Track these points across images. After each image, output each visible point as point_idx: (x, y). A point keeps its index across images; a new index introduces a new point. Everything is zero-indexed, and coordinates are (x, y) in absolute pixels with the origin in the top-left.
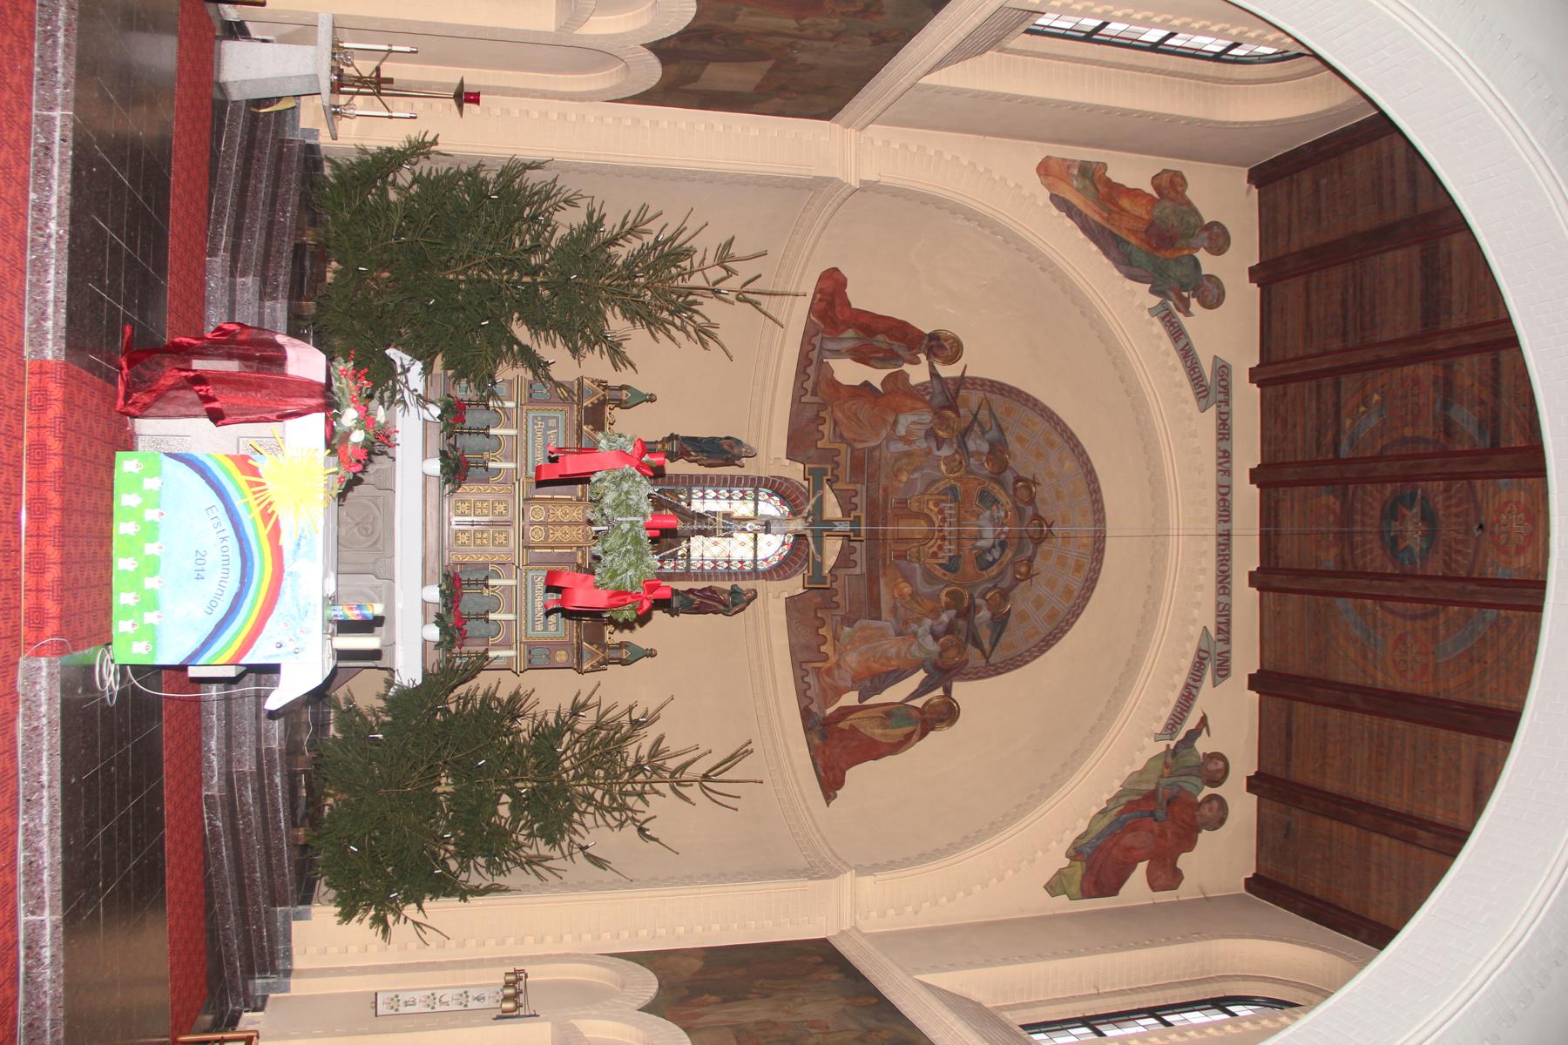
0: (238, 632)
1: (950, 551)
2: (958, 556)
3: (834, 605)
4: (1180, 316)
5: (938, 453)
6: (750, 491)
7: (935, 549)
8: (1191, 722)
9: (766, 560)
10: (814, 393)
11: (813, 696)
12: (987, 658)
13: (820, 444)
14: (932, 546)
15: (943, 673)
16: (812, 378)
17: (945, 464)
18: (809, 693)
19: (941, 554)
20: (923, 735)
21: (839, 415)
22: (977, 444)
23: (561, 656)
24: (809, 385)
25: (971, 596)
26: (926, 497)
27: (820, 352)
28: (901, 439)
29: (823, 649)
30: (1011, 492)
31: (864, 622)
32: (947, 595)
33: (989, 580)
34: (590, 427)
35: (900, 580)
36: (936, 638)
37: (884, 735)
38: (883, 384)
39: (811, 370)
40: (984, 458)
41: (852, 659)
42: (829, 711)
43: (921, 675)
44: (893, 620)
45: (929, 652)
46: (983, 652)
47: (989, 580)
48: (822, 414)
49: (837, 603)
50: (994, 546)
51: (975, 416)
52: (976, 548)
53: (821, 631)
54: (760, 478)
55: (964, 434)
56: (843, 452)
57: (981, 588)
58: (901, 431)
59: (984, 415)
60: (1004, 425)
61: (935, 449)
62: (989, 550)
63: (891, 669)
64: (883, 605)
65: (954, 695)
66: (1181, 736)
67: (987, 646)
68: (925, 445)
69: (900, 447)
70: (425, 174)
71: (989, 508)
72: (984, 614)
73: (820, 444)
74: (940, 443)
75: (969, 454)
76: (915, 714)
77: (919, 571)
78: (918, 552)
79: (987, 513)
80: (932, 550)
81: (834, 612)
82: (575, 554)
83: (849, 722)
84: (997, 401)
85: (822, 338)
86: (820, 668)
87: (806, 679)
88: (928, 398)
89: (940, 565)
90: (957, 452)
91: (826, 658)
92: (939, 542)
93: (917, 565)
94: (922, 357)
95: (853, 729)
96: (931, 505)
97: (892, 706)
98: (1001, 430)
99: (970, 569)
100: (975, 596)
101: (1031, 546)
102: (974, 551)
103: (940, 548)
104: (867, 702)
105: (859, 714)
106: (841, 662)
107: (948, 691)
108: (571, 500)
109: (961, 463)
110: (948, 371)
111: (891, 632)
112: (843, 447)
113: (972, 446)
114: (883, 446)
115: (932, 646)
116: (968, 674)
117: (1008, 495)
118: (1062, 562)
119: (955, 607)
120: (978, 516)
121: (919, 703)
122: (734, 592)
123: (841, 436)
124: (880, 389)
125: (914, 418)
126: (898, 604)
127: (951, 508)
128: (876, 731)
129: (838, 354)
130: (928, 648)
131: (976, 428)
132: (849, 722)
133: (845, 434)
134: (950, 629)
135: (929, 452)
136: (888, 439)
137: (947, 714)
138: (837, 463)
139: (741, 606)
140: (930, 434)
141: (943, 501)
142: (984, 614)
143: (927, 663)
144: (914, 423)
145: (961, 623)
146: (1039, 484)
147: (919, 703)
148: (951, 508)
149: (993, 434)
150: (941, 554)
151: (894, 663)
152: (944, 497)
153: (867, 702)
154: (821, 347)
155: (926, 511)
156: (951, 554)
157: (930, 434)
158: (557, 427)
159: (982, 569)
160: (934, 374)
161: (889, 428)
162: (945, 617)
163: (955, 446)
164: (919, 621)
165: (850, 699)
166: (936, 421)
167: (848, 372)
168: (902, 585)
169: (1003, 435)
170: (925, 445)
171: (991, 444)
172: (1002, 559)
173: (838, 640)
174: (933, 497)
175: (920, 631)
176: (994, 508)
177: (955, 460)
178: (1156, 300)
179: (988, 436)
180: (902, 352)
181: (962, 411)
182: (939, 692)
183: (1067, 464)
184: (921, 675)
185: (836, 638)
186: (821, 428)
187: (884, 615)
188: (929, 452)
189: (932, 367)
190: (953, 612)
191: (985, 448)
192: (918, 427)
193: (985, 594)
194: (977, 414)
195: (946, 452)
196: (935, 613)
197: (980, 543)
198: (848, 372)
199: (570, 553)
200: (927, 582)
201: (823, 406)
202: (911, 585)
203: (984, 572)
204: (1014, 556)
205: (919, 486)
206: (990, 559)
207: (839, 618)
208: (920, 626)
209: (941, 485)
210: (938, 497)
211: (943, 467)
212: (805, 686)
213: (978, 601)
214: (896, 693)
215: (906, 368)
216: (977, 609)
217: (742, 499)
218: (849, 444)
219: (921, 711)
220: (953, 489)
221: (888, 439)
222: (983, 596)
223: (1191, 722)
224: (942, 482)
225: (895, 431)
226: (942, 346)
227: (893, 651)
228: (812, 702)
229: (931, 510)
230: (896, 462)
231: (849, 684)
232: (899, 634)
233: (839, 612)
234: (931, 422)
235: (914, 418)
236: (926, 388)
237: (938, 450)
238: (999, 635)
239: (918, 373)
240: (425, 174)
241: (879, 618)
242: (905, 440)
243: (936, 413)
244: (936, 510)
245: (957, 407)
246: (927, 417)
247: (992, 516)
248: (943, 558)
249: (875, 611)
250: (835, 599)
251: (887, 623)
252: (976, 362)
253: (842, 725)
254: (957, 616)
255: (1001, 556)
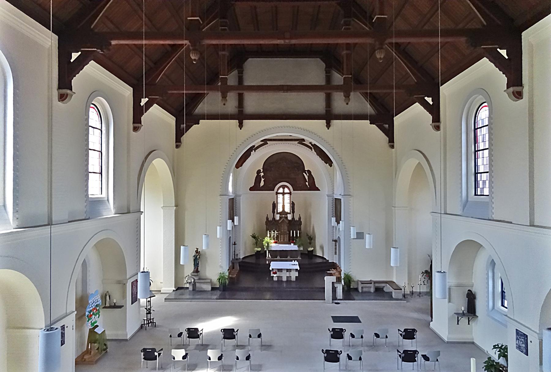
4: (255, 147)
8: (310, 145)
15: (305, 171)
22: (272, 165)
38: (263, 178)
65: (307, 170)
66: (312, 147)
70: (197, 55)
104: (308, 181)
107: (306, 171)
110: (262, 171)
115: (300, 172)
121: (308, 175)
122: (292, 204)
134: (298, 169)
137: (309, 172)
142: (296, 165)
147: (308, 175)
165: (307, 183)
167: (262, 184)
178: (253, 151)
182: (306, 172)
198: (262, 184)
214: (307, 178)
215: (261, 176)
223: (310, 145)
226: (259, 172)
239: (262, 174)
240: (197, 55)
252: (261, 168)
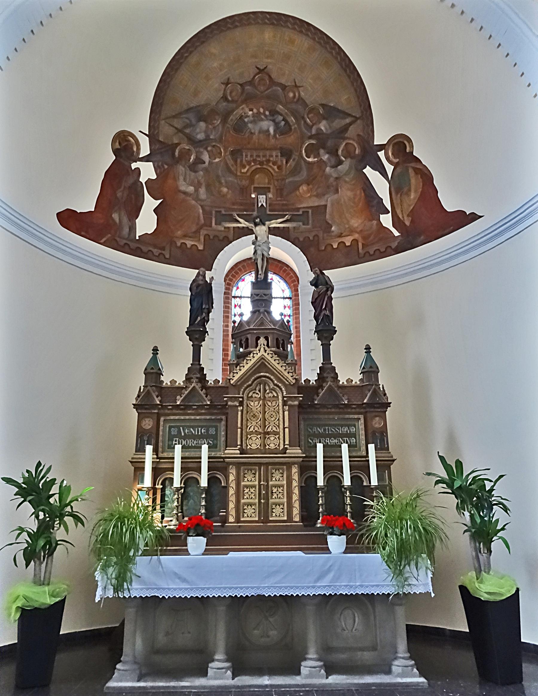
0: (281, 554)
1: (277, 156)
2: (281, 149)
3: (316, 238)
5: (207, 163)
6: (234, 301)
7: (275, 167)
9: (283, 291)
10: (163, 249)
11: (385, 246)
12: (357, 119)
13: (201, 247)
14: (274, 169)
16: (151, 249)
17: (215, 159)
18: (383, 250)
19: (279, 163)
20: (418, 160)
21: (179, 233)
23: (377, 423)
24: (156, 252)
25: (310, 137)
26: (239, 174)
27: (131, 241)
28: (196, 190)
29: (348, 244)
30: (234, 105)
31: (328, 216)
32: (309, 158)
33: (299, 125)
34: (178, 397)
35: (298, 193)
36: (340, 163)
37: (416, 191)
39: (145, 249)
40: (210, 126)
41: (356, 223)
42: (396, 233)
43: (368, 171)
44: (326, 197)
45: (350, 167)
46: (350, 124)
47: (299, 125)
48: (179, 244)
49: (314, 237)
50: (274, 121)
51: (179, 131)
52: (275, 135)
53: (335, 246)
54: (225, 293)
55: (191, 140)
56: (205, 232)
57: (304, 129)
58: (191, 189)
59: (178, 123)
60: (185, 107)
61: (204, 165)
62: (276, 124)
63: (363, 194)
64: (316, 204)
67: (348, 120)
68: (201, 173)
69: (202, 191)
71: (246, 124)
72: (323, 126)
73: (201, 247)
74: (199, 161)
75: (207, 138)
76: (399, 170)
77: (291, 179)
78: (277, 180)
79: (250, 125)
80: (277, 170)
81: (321, 238)
82: (290, 406)
83: (406, 218)
84: (167, 110)
85: (119, 237)
86: (363, 244)
87: (372, 253)
88: (166, 167)
89: (287, 163)
90: (206, 149)
91: (355, 241)
92: (271, 164)
93: (287, 181)
94: (134, 166)
95: (411, 214)
96: (246, 170)
97: (392, 189)
98: (189, 110)
99: (291, 139)
100: (309, 134)
101: (274, 88)
102: (277, 136)
103: (274, 163)
104: (390, 209)
105: (398, 211)
106: (359, 230)
107: (381, 147)
108: (242, 411)
109: (214, 146)
111: (336, 196)
112: (203, 232)
113: (201, 136)
114: (202, 204)
116: (369, 134)
117: (237, 108)
118: (287, 57)
119: (318, 150)
120: (252, 133)
121: (389, 169)
123: (195, 232)
124: (160, 201)
125: (181, 178)
126: (315, 193)
127: (246, 156)
128: (412, 197)
129: (133, 228)
130: (347, 168)
131: (187, 131)
132: (406, 218)
133: (194, 230)
135: (206, 170)
136: (197, 199)
138: (215, 236)
139: (327, 279)
140: (193, 168)
141: (241, 161)
142: (323, 126)
143: (359, 167)
144: (185, 180)
145: (330, 143)
146: (228, 79)
147: (389, 169)
148: (246, 156)
149: (192, 116)
150: (279, 163)
151: (358, 192)
152: (239, 160)
153: (390, 209)
154: (126, 239)
155: (248, 174)
156: (279, 154)
157: (193, 168)
158: (178, 427)
159: (291, 129)
160: (146, 159)
161: (188, 198)
162: (325, 157)
163: (202, 150)
164: (328, 177)
165: (386, 220)
166: (183, 162)
168: (301, 191)
169: (191, 108)
170: (201, 173)
171: (200, 119)
172: (283, 113)
173: (342, 234)
174: (239, 169)
175: (335, 175)
176: (246, 120)
177: (212, 151)
179: (194, 121)
180: (131, 181)
181: (176, 141)
182: (381, 154)
183: (213, 50)
184: (368, 171)
185: (340, 236)
186: (189, 246)
187: (323, 203)
188: (206, 170)
189: (142, 160)
190: (322, 151)
191: (202, 124)
192: (188, 177)
193: (307, 124)
194: (176, 128)
195: (206, 157)
196: (321, 164)
197: (272, 130)
199: (289, 410)
200: (300, 172)
201: (172, 243)
202: (301, 185)
203: (293, 128)
204: (281, 103)
205: (230, 179)
206: (283, 123)
207: (325, 235)
208: (332, 176)
209: (230, 162)
210: (238, 165)
211: (217, 160)
212: (377, 252)
213: (314, 131)
215: (143, 179)
216: (319, 132)
217: (240, 306)
218: (201, 228)
219: (396, 165)
220: (233, 153)
221: (197, 199)
222: (310, 127)
224: (228, 162)
225: (191, 194)
227: (349, 194)
228: (390, 247)
229: (248, 170)
230: (214, 195)
231: (375, 222)
232: (337, 191)
233: (321, 235)
234: (184, 167)
235: (181, 178)
236: (158, 166)
237: (204, 163)
238: (339, 111)
241: (325, 206)
242: (197, 186)
243: (178, 162)
244: (247, 167)
245: (172, 144)
246: (181, 169)
247: (251, 122)
248: (282, 161)
249: (321, 210)
250: (311, 238)
251: (329, 200)
253: (408, 223)
254: (324, 148)
255: (281, 115)
